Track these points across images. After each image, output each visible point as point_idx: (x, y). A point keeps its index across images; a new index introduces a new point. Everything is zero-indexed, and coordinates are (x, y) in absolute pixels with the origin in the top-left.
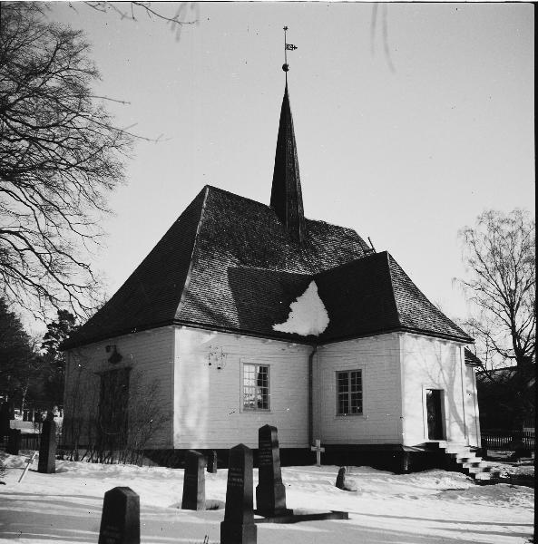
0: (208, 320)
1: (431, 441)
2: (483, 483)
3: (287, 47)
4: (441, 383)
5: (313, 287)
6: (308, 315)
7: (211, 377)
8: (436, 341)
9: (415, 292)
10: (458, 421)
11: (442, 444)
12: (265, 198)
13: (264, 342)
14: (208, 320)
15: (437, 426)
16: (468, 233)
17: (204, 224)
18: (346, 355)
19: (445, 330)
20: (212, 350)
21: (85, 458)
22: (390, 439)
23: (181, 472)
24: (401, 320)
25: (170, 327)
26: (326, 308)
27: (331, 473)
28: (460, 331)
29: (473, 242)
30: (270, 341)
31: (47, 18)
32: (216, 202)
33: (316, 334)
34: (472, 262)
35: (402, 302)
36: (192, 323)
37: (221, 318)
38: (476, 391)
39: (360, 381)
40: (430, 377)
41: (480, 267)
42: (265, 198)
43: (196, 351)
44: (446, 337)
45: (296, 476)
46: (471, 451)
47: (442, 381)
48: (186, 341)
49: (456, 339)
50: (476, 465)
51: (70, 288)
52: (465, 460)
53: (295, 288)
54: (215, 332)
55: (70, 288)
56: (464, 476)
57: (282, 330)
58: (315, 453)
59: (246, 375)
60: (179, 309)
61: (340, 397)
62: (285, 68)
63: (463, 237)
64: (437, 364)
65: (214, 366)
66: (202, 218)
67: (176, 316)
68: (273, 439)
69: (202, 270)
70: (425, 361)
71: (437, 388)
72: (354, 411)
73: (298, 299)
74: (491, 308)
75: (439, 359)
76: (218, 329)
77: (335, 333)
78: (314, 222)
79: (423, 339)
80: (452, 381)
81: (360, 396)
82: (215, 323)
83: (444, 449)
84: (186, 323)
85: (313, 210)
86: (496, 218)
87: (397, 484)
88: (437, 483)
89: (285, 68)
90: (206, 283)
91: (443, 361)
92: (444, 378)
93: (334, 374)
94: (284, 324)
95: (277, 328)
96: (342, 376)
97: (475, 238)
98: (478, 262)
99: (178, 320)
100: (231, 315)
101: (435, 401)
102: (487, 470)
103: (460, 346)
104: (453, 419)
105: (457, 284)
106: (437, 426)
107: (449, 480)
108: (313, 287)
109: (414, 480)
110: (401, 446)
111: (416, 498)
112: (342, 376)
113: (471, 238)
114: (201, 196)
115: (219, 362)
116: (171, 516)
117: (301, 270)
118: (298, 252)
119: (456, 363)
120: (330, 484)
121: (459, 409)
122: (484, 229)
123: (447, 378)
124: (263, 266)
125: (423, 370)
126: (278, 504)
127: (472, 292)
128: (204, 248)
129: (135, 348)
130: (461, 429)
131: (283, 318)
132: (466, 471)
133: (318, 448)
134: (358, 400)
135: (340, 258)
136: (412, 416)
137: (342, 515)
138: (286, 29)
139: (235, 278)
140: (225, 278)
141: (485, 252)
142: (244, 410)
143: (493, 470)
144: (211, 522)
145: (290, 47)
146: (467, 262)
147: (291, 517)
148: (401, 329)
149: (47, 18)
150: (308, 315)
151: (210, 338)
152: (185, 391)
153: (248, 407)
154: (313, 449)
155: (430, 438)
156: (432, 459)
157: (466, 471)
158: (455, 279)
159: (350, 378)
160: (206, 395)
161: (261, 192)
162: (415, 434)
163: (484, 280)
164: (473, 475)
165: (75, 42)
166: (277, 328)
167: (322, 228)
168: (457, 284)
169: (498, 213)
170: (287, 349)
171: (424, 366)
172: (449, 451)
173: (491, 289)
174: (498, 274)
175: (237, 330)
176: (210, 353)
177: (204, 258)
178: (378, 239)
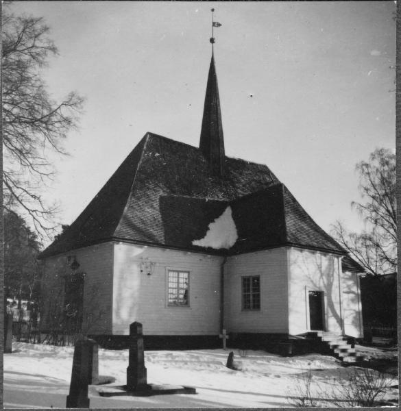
0: (138, 237)
1: (313, 331)
2: (347, 365)
3: (214, 24)
4: (321, 284)
5: (228, 211)
6: (221, 233)
7: (142, 281)
8: (318, 254)
9: (302, 215)
10: (335, 315)
11: (320, 334)
12: (195, 141)
13: (185, 254)
14: (138, 237)
15: (318, 319)
16: (364, 167)
17: (143, 163)
18: (248, 265)
19: (323, 244)
20: (144, 260)
21: (45, 341)
22: (277, 329)
23: (126, 353)
24: (289, 239)
25: (111, 243)
26: (237, 228)
27: (221, 356)
28: (337, 245)
29: (368, 173)
30: (189, 253)
31: (10, 9)
32: (155, 142)
33: (227, 247)
34: (367, 190)
35: (290, 222)
36: (127, 239)
37: (151, 237)
38: (359, 291)
39: (258, 284)
40: (312, 281)
41: (372, 192)
42: (195, 141)
43: (130, 261)
44: (325, 251)
45: (197, 357)
46: (344, 339)
47: (322, 284)
48: (122, 252)
49: (334, 252)
50: (344, 351)
51: (34, 214)
52: (336, 347)
53: (214, 212)
54: (146, 247)
55: (34, 214)
56: (334, 359)
57: (199, 245)
58: (222, 339)
59: (171, 279)
60: (117, 229)
61: (244, 296)
62: (212, 41)
63: (360, 170)
64: (318, 271)
65: (145, 273)
66: (142, 158)
67: (115, 235)
68: (138, 333)
69: (139, 199)
70: (308, 269)
71: (317, 289)
72: (254, 307)
73: (216, 220)
74: (382, 226)
75: (320, 267)
76: (148, 244)
77: (238, 249)
78: (233, 161)
79: (306, 253)
80: (329, 286)
81: (259, 295)
82: (143, 239)
83: (321, 338)
84: (125, 240)
85: (234, 148)
86: (386, 154)
87: (283, 366)
88: (309, 364)
89: (212, 41)
90: (141, 210)
91: (323, 269)
92: (324, 282)
93: (240, 279)
94: (202, 240)
95: (196, 243)
96: (246, 281)
97: (370, 171)
98: (373, 190)
99: (116, 238)
100: (159, 234)
101: (317, 302)
102: (352, 355)
103: (338, 258)
104: (330, 314)
105: (356, 207)
106: (318, 319)
107: (318, 362)
108: (228, 211)
109: (291, 362)
110: (287, 335)
111: (279, 377)
112: (246, 281)
113: (366, 170)
114: (143, 140)
115: (149, 270)
116: (50, 389)
117: (220, 197)
118: (220, 184)
119: (334, 270)
120: (221, 364)
121: (337, 307)
122: (376, 163)
123: (326, 282)
124: (189, 195)
125: (307, 276)
126: (140, 381)
127: (367, 213)
128: (142, 181)
129: (88, 258)
130: (338, 322)
131: (201, 234)
132: (336, 356)
133: (225, 336)
134: (257, 298)
135: (253, 188)
136: (297, 312)
137: (190, 390)
138: (213, 10)
139: (165, 205)
140: (156, 205)
141: (377, 181)
142: (168, 306)
143: (358, 354)
144: (8, 404)
145: (216, 24)
146: (363, 190)
147: (149, 391)
148: (289, 245)
149: (10, 9)
150: (221, 233)
151: (138, 251)
152: (120, 289)
153: (175, 304)
154: (221, 336)
155: (312, 329)
156: (312, 345)
157: (336, 356)
158: (353, 203)
159: (251, 282)
160: (136, 294)
161: (192, 137)
162: (299, 324)
163: (376, 204)
164: (341, 359)
165: (38, 26)
166: (196, 243)
167: (240, 164)
168: (356, 207)
169: (387, 151)
170: (204, 260)
171: (306, 273)
172: (325, 339)
173: (382, 210)
174: (387, 199)
175: (163, 245)
176: (141, 261)
177: (141, 189)
178: (283, 174)
